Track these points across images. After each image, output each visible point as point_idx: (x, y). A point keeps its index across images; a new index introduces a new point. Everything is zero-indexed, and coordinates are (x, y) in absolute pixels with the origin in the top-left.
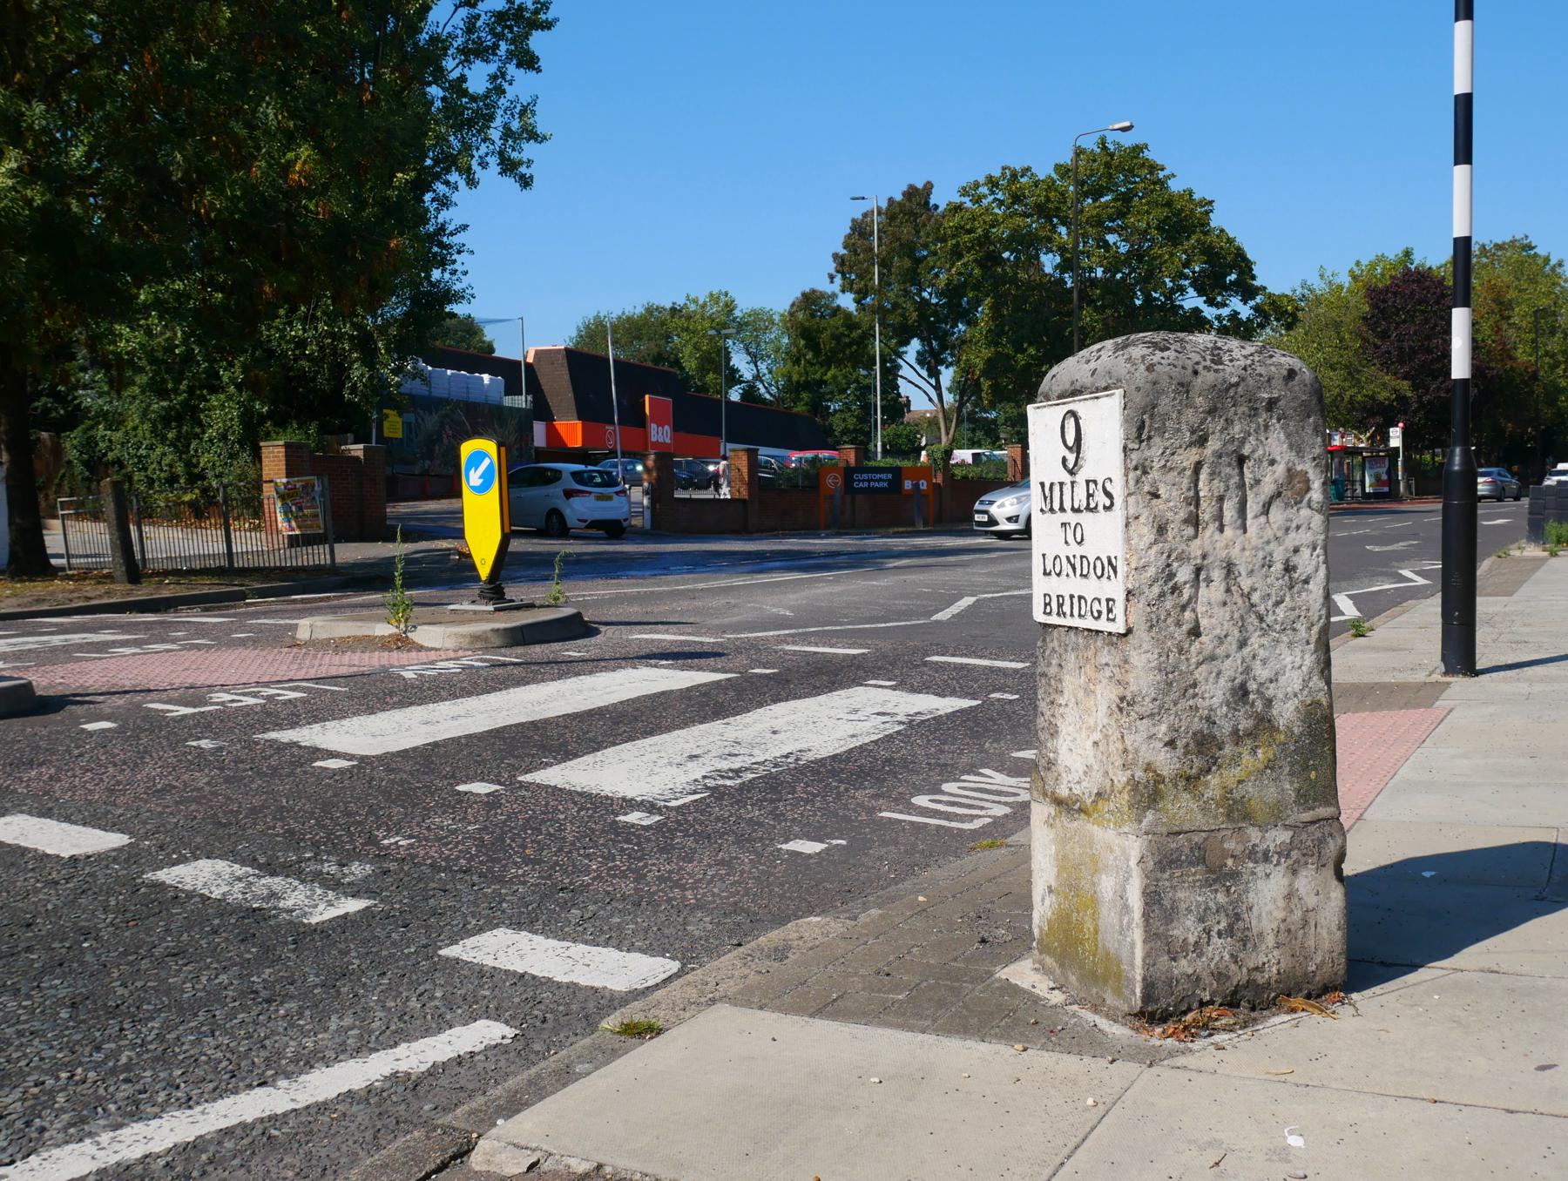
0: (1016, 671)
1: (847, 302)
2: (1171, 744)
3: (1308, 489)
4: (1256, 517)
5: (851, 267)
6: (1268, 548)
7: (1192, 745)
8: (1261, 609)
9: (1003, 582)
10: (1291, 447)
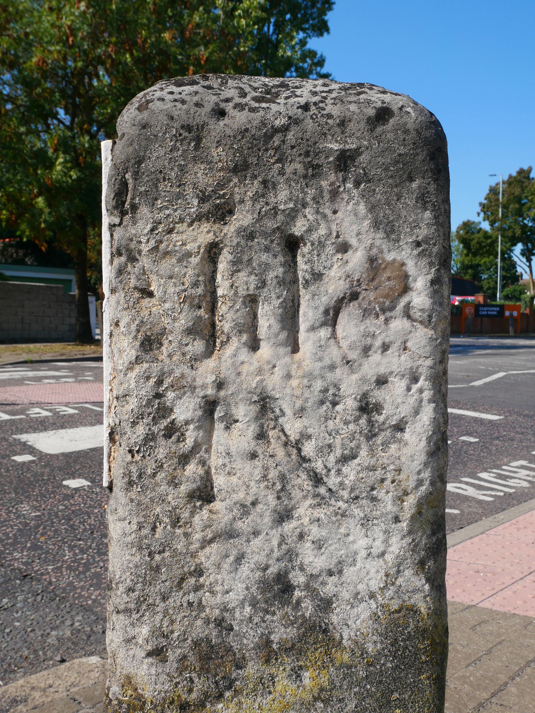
0: (490, 421)
1: (486, 226)
2: (158, 653)
3: (406, 289)
4: (313, 329)
5: (488, 209)
6: (330, 376)
7: (192, 658)
8: (319, 466)
9: (529, 364)
10: (376, 225)
